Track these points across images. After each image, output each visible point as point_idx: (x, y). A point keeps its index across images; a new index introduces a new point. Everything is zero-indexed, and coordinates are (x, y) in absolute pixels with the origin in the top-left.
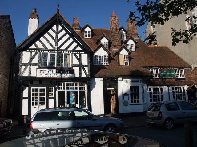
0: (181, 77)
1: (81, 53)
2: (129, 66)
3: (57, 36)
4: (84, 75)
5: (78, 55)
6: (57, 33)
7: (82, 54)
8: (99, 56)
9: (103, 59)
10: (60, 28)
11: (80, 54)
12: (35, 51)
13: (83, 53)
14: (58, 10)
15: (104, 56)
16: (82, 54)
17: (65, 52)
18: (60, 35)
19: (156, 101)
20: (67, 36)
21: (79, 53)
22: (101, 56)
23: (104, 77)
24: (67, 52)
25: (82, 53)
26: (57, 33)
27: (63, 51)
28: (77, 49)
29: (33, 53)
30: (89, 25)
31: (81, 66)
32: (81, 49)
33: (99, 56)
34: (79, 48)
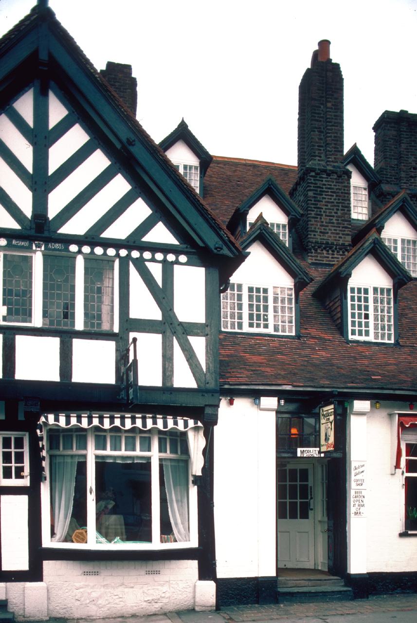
0: (251, 325)
1: (171, 257)
2: (397, 343)
3: (41, 158)
4: (184, 379)
5: (156, 270)
7: (176, 267)
8: (251, 290)
10: (57, 112)
11: (164, 262)
13: (183, 258)
15: (375, 289)
16: (176, 267)
17: (86, 249)
21: (159, 256)
22: (258, 290)
24: (99, 251)
25: (177, 262)
27: (80, 241)
28: (149, 238)
30: (193, 129)
32: (169, 239)
33: (251, 290)
34: (161, 234)
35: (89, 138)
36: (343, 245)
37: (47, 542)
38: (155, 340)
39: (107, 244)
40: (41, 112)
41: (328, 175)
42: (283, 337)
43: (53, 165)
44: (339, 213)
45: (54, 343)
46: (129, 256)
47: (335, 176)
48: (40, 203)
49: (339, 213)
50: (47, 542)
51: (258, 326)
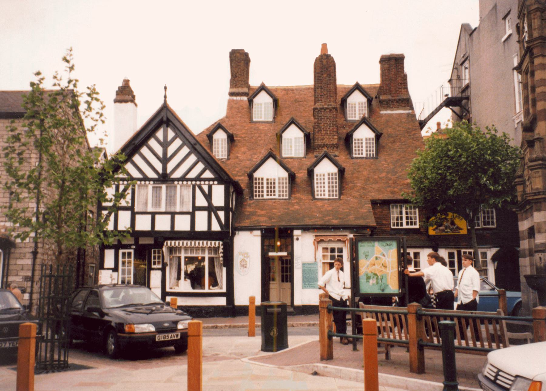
0: (268, 195)
1: (211, 183)
4: (216, 227)
5: (206, 188)
6: (165, 145)
8: (268, 180)
9: (364, 145)
10: (171, 134)
12: (125, 182)
13: (216, 182)
14: (165, 97)
18: (171, 150)
19: (492, 225)
20: (185, 150)
21: (207, 183)
23: (261, 230)
25: (214, 184)
26: (165, 145)
27: (178, 180)
28: (204, 176)
29: (122, 188)
31: (211, 209)
34: (208, 174)
35: (100, 271)
36: (333, 144)
37: (168, 290)
38: (205, 214)
39: (188, 180)
40: (165, 136)
41: (325, 110)
42: (283, 199)
43: (169, 155)
44: (331, 128)
45: (169, 217)
46: (196, 184)
47: (328, 110)
48: (165, 168)
49: (331, 128)
50: (168, 290)
51: (271, 195)
